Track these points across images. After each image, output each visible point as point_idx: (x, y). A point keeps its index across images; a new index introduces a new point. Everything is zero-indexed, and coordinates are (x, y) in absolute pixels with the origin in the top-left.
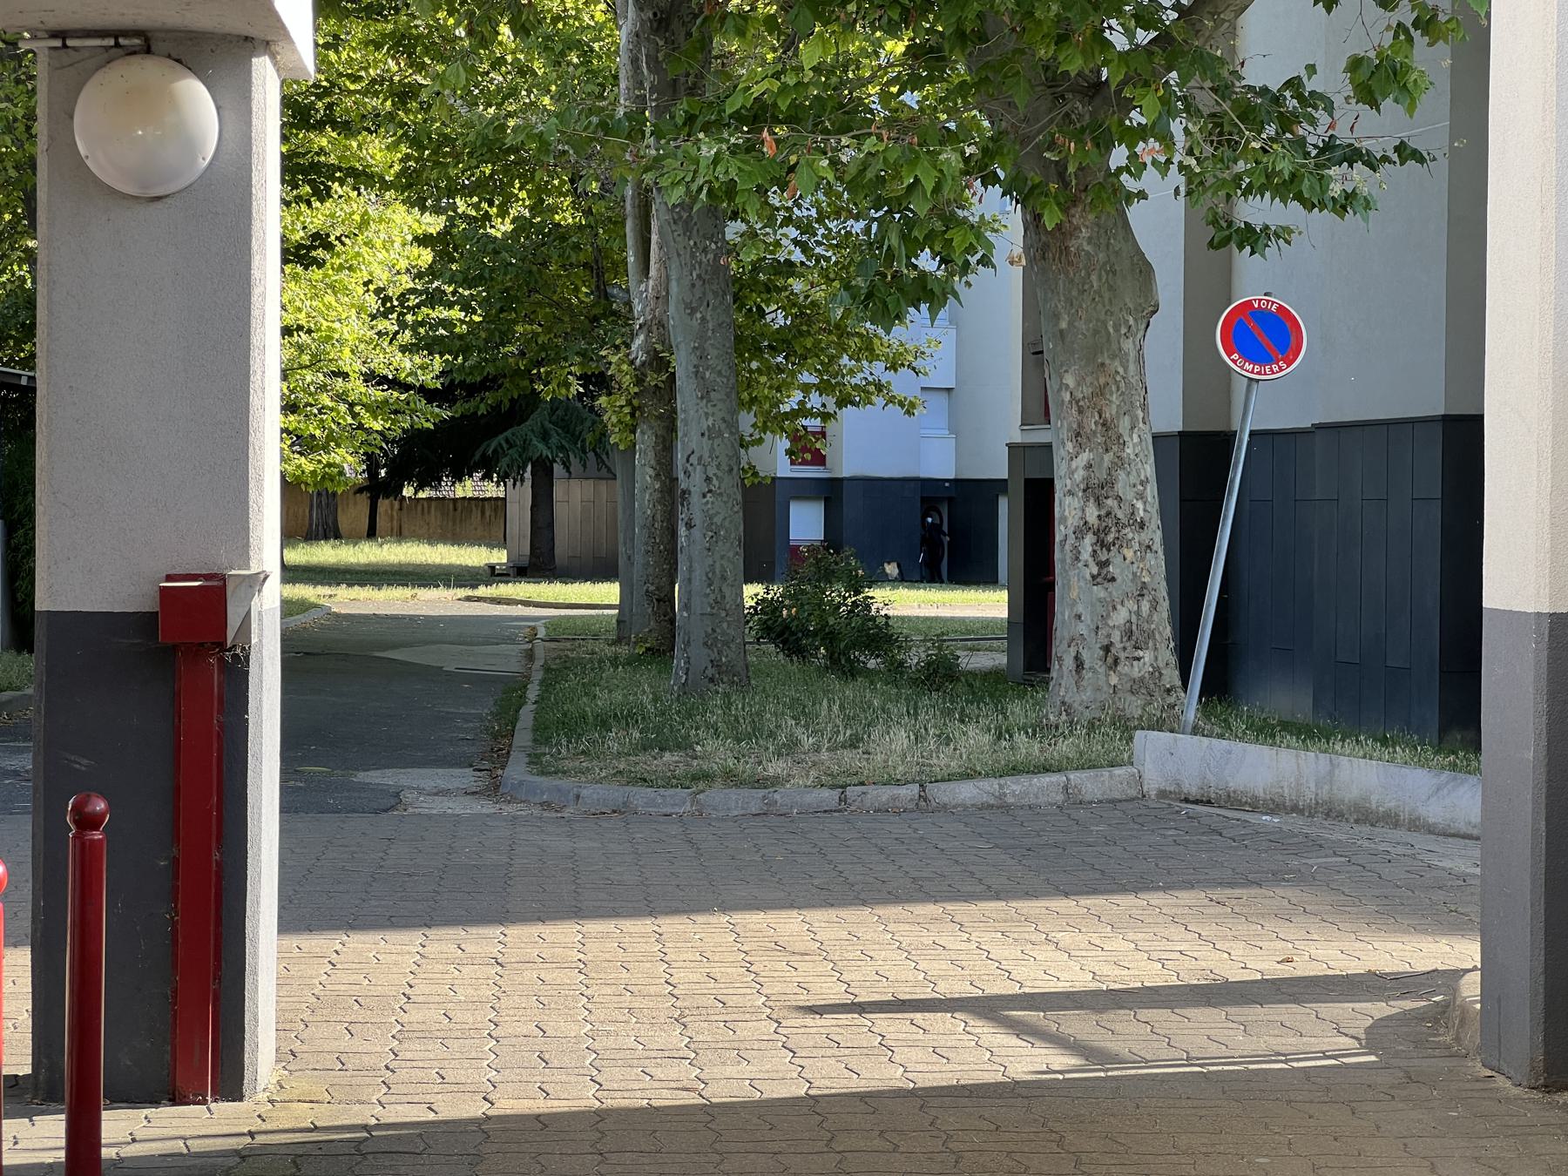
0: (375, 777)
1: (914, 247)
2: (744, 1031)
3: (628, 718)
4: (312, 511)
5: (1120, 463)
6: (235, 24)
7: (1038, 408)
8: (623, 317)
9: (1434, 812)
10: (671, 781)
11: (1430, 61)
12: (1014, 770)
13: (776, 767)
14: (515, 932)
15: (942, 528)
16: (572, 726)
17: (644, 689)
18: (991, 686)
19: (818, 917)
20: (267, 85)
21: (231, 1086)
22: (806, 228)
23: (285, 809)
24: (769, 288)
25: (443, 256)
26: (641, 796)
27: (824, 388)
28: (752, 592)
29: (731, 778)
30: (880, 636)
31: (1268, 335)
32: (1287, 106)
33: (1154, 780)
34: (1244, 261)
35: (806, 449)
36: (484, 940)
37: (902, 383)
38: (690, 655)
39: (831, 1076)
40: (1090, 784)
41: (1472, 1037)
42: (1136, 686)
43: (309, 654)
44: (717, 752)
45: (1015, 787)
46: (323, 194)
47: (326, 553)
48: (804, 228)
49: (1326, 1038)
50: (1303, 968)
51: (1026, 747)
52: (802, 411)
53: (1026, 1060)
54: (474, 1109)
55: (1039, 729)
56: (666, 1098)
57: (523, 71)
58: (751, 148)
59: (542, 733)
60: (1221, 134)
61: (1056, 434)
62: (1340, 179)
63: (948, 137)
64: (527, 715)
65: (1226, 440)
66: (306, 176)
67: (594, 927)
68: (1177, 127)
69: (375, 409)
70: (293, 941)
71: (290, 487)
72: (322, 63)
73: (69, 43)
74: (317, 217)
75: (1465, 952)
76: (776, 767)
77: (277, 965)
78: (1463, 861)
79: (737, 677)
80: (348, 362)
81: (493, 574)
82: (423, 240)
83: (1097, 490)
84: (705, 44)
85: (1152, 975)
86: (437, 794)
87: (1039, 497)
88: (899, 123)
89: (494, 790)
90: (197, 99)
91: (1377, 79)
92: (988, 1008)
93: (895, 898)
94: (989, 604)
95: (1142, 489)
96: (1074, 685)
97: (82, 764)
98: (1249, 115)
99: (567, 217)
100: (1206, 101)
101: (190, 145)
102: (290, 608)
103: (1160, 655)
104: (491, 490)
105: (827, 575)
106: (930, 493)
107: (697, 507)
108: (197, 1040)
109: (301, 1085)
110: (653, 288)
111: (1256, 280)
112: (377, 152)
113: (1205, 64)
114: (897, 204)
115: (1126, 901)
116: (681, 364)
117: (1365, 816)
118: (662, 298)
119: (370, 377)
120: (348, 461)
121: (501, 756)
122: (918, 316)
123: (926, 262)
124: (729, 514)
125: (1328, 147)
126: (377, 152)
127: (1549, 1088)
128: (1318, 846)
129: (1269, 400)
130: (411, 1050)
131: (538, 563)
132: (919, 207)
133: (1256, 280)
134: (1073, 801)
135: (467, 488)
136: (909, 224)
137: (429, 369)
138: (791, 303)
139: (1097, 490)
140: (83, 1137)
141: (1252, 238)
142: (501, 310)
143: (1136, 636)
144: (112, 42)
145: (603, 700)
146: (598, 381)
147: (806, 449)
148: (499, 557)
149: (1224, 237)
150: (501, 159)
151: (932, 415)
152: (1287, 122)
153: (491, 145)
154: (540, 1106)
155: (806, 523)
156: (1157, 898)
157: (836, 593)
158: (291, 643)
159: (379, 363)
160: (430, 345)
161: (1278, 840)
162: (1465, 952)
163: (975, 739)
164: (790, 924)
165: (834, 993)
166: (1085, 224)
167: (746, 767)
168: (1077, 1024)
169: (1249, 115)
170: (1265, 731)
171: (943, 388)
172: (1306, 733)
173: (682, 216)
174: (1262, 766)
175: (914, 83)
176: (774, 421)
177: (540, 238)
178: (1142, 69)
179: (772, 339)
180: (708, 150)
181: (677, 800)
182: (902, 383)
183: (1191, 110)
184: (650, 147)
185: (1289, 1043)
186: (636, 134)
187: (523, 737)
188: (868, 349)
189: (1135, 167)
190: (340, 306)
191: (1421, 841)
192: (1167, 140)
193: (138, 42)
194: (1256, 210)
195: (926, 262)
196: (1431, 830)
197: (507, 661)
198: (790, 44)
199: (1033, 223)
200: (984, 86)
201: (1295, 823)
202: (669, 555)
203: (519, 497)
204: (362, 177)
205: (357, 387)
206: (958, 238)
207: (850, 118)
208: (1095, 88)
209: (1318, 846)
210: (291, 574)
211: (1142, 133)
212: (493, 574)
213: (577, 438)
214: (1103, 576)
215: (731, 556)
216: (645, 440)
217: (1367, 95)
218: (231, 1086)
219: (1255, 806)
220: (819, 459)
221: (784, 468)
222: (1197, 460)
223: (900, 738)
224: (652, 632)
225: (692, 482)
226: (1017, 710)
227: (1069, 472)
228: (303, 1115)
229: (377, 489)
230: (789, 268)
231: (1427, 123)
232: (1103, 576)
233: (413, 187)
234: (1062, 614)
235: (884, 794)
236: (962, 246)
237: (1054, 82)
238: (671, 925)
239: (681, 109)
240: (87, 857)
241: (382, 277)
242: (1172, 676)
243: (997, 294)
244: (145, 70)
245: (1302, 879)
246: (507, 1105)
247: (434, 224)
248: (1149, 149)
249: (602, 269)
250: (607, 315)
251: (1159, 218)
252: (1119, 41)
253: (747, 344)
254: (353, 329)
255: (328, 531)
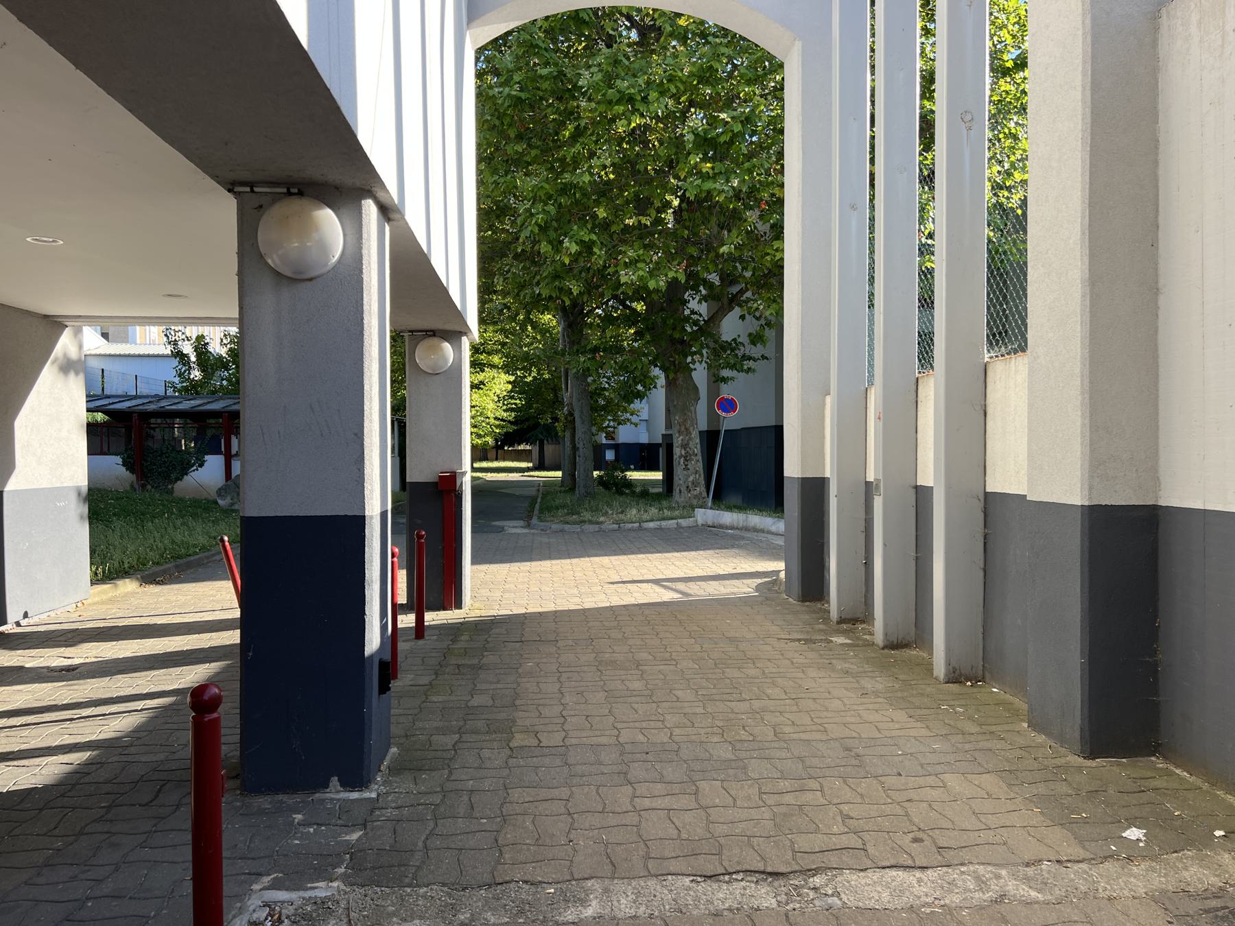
0: (497, 523)
1: (636, 384)
2: (594, 589)
3: (563, 507)
4: (480, 453)
5: (690, 439)
6: (458, 328)
7: (669, 425)
8: (562, 403)
9: (773, 529)
10: (575, 523)
11: (770, 334)
12: (664, 519)
13: (602, 519)
14: (534, 563)
15: (645, 456)
16: (549, 509)
17: (568, 499)
18: (658, 497)
19: (613, 558)
20: (466, 343)
21: (459, 605)
22: (609, 378)
23: (473, 532)
24: (600, 395)
25: (514, 387)
26: (567, 527)
27: (614, 420)
28: (596, 473)
29: (591, 522)
30: (630, 484)
31: (729, 405)
32: (733, 346)
33: (700, 522)
34: (723, 386)
35: (610, 436)
36: (526, 566)
37: (634, 419)
38: (580, 490)
39: (616, 601)
40: (684, 522)
41: (783, 587)
42: (695, 497)
43: (478, 490)
44: (587, 515)
45: (664, 523)
46: (483, 371)
47: (484, 464)
48: (608, 380)
49: (746, 588)
50: (739, 570)
51: (667, 513)
52: (608, 426)
53: (667, 596)
54: (523, 611)
55: (670, 508)
56: (573, 607)
57: (534, 338)
58: (594, 358)
59: (541, 511)
60: (716, 353)
61: (674, 432)
62: (747, 364)
63: (645, 355)
64: (537, 506)
65: (718, 432)
66: (477, 365)
67: (554, 562)
68: (704, 351)
69: (497, 427)
70: (475, 567)
71: (474, 447)
72: (481, 336)
73: (256, 189)
74: (481, 377)
75: (781, 565)
76: (602, 519)
77: (470, 571)
78: (780, 541)
79: (590, 495)
80: (489, 414)
81: (528, 469)
82: (509, 382)
83: (684, 446)
84: (581, 331)
85: (700, 573)
86: (514, 528)
87: (670, 448)
88: (632, 351)
89: (528, 526)
90: (447, 347)
91: (756, 339)
92: (657, 582)
93: (633, 553)
94: (658, 476)
95: (696, 446)
96: (678, 498)
97: (419, 522)
98: (723, 348)
99: (546, 376)
100: (712, 345)
101: (446, 360)
102: (473, 479)
103: (701, 489)
104: (528, 447)
105: (615, 469)
106: (641, 447)
107: (581, 451)
108: (450, 594)
109: (477, 605)
110: (569, 394)
111: (726, 391)
112: (496, 359)
113: (710, 335)
114: (632, 372)
115: (693, 553)
116: (577, 415)
117: (755, 530)
118: (571, 397)
119: (496, 418)
120: (490, 440)
121: (530, 517)
122: (637, 401)
123: (640, 387)
124: (590, 454)
125: (744, 356)
126: (496, 359)
127: (803, 601)
128: (743, 538)
129: (730, 421)
130: (507, 595)
131: (540, 467)
132: (637, 373)
133: (726, 391)
134: (679, 526)
135: (521, 447)
136: (635, 378)
137: (511, 416)
138: (605, 398)
139: (684, 446)
140: (420, 619)
141: (725, 380)
142: (528, 401)
143: (695, 484)
144: (285, 190)
145: (557, 502)
146: (556, 419)
147: (610, 436)
148: (530, 465)
149: (717, 380)
150: (528, 361)
151: (643, 427)
152: (733, 350)
153: (526, 357)
154: (540, 610)
155: (610, 455)
156: (701, 552)
157: (618, 474)
158: (473, 488)
159: (497, 414)
160: (512, 410)
161: (733, 537)
162: (781, 565)
163: (653, 511)
164: (605, 560)
165: (617, 579)
166: (680, 376)
167: (594, 519)
168: (681, 586)
169: (723, 348)
170: (729, 508)
171: (645, 420)
172: (739, 508)
173: (576, 376)
174: (728, 518)
175: (636, 341)
176: (601, 429)
177: (538, 384)
178: (695, 336)
179: (602, 408)
180: (582, 359)
181: (577, 528)
182: (634, 419)
183: (708, 347)
184: (567, 358)
185: (736, 590)
186: (563, 355)
187: (536, 512)
188: (625, 410)
189: (693, 362)
190: (488, 400)
191: (770, 536)
192: (702, 355)
193: (432, 333)
194: (726, 373)
195: (640, 387)
196: (772, 533)
197: (532, 491)
198: (604, 331)
199: (667, 377)
200: (653, 341)
201: (737, 532)
202: (574, 464)
203: (535, 449)
204: (493, 366)
205: (492, 421)
206: (647, 381)
207: (620, 350)
208: (682, 342)
209: (743, 538)
210: (474, 470)
211: (695, 353)
212: (528, 469)
213: (550, 433)
214: (686, 469)
215: (591, 464)
216: (568, 434)
217: (753, 343)
218: (459, 605)
219: (727, 528)
220: (613, 439)
221: (604, 441)
222: (710, 438)
223: (634, 511)
224: (570, 483)
225: (580, 445)
226: (665, 503)
227: (678, 441)
228: (478, 613)
229: (498, 447)
230: (605, 389)
231: (769, 350)
232: (686, 469)
233: (507, 369)
234: (676, 478)
235: (630, 526)
236: (649, 383)
237: (673, 341)
238: (575, 561)
239: (575, 348)
240: (420, 546)
241: (498, 392)
242: (705, 494)
243: (659, 395)
244: (435, 341)
245: (739, 547)
246: (531, 610)
247: (512, 378)
248: (696, 357)
249: (556, 390)
250: (557, 402)
251: (700, 375)
252: (689, 329)
253: (594, 408)
254: (491, 406)
255: (485, 459)
